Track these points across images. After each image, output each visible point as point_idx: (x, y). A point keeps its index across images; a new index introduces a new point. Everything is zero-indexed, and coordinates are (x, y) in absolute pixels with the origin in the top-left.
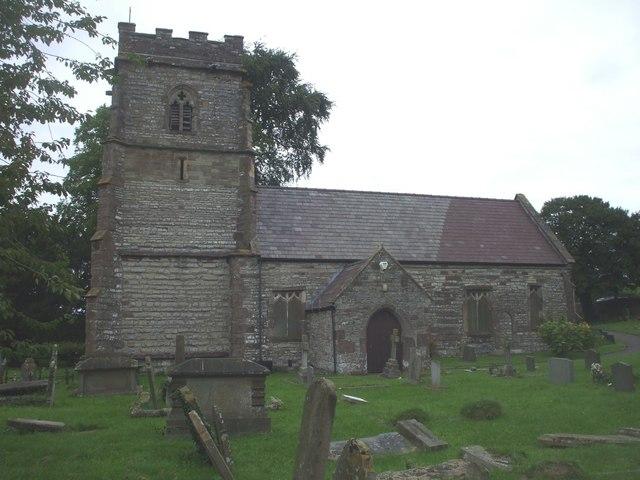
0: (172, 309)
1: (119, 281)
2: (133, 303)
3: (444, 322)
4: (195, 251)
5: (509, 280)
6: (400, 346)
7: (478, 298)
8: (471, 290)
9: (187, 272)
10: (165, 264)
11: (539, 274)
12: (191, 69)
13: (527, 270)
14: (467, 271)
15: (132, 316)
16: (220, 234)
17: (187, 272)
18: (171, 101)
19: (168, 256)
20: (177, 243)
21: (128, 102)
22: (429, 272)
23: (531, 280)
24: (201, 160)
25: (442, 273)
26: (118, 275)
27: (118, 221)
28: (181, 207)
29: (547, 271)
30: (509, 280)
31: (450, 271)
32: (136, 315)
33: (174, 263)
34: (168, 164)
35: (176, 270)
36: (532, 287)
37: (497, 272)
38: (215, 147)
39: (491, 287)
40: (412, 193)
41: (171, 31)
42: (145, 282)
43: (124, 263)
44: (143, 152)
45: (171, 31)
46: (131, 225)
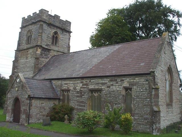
7: (96, 95)
11: (132, 81)
12: (31, 24)
13: (123, 79)
14: (92, 81)
22: (76, 82)
23: (126, 84)
25: (81, 82)
27: (16, 72)
28: (26, 66)
29: (136, 79)
30: (112, 85)
31: (84, 81)
36: (126, 89)
37: (106, 81)
44: (22, 52)
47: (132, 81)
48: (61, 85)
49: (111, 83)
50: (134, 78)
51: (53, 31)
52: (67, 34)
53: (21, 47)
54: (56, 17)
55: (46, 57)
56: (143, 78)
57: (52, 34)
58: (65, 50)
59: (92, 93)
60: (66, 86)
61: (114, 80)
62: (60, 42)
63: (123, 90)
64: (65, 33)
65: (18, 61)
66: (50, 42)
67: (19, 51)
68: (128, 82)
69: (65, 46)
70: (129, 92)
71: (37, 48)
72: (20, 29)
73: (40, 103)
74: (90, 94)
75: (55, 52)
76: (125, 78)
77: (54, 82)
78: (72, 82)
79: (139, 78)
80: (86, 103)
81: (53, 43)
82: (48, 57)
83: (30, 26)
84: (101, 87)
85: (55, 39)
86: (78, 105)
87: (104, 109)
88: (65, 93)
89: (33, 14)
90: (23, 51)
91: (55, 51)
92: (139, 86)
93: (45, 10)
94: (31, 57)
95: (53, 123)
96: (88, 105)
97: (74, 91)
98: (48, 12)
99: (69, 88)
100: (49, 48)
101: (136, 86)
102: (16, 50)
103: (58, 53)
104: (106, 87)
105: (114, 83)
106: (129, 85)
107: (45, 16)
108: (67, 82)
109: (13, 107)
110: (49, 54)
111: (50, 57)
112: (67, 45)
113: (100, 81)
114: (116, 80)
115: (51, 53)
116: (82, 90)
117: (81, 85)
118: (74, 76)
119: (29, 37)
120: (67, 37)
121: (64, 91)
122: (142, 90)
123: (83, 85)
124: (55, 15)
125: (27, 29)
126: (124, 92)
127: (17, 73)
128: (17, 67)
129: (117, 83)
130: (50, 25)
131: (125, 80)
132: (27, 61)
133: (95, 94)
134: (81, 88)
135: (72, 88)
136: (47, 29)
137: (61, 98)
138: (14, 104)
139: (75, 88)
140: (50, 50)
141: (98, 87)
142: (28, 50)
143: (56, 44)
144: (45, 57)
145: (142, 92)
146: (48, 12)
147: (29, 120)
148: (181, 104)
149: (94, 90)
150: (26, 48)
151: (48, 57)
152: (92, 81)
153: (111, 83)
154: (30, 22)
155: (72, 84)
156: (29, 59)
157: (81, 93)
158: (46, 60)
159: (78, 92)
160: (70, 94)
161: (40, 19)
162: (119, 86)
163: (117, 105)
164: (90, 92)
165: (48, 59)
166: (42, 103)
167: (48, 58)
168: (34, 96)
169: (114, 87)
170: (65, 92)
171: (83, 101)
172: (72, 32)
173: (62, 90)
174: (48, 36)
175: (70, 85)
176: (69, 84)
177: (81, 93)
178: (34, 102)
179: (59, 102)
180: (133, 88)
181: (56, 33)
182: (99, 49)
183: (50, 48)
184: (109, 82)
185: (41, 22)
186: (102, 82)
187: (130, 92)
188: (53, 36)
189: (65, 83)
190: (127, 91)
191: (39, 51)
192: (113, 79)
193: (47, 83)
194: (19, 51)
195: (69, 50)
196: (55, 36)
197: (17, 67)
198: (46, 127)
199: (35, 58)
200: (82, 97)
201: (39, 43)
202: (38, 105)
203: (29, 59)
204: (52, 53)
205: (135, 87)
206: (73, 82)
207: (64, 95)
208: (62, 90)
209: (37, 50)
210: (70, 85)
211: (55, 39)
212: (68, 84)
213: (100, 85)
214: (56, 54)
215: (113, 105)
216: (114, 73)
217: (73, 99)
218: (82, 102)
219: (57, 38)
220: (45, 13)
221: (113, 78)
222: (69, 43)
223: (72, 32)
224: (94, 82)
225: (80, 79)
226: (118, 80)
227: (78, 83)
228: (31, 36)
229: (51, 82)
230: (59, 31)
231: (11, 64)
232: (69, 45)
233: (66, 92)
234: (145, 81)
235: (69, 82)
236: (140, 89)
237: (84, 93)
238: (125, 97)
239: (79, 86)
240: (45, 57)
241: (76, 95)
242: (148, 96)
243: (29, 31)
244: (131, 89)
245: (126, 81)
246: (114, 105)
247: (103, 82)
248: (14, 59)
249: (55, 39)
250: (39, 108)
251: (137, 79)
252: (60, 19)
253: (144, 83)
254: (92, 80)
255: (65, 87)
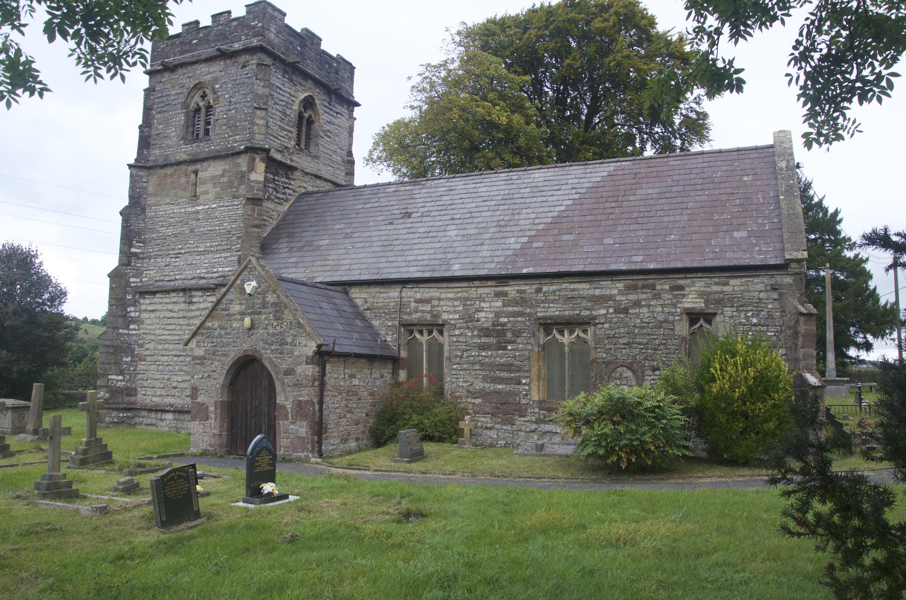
0: (178, 353)
1: (134, 321)
2: (147, 346)
3: (495, 380)
4: (203, 281)
5: (637, 304)
6: (179, 541)
7: (566, 339)
8: (547, 325)
9: (193, 308)
10: (175, 300)
11: (715, 288)
12: (209, 60)
13: (681, 282)
14: (545, 289)
15: (145, 361)
16: (225, 258)
17: (193, 308)
18: (193, 106)
19: (174, 290)
20: (189, 273)
21: (154, 118)
22: (473, 293)
23: (692, 301)
24: (214, 169)
25: (497, 295)
26: (132, 314)
27: (135, 254)
28: (192, 231)
29: (733, 282)
30: (637, 304)
31: (512, 290)
32: (148, 359)
33: (180, 297)
34: (183, 180)
35: (183, 306)
36: (693, 317)
37: (613, 288)
38: (229, 149)
39: (594, 318)
40: (363, 184)
41: (229, 12)
42: (157, 321)
43: (142, 301)
44: (163, 172)
45: (229, 12)
46: (149, 258)
47: (715, 288)
48: (402, 305)
49: (633, 297)
50: (723, 280)
51: (302, 97)
52: (344, 110)
53: (156, 154)
54: (309, 39)
55: (279, 198)
56: (756, 280)
57: (296, 107)
58: (338, 172)
59: (548, 332)
60: (428, 308)
61: (644, 287)
62: (324, 145)
63: (681, 320)
64: (339, 108)
65: (143, 210)
66: (290, 138)
67: (141, 167)
68: (701, 294)
69: (339, 158)
70: (701, 326)
71: (254, 159)
72: (148, 77)
73: (347, 376)
74: (542, 339)
75: (307, 179)
76: (689, 281)
77: (355, 293)
78: (451, 295)
79: (743, 280)
80: (527, 368)
81: (298, 143)
82: (284, 197)
83: (203, 69)
84: (588, 313)
85: (304, 129)
86: (485, 379)
87: (488, 409)
88: (418, 336)
89: (215, 17)
90: (169, 171)
91: (307, 174)
92: (741, 306)
93: (274, 8)
94: (218, 197)
95: (429, 447)
96: (534, 377)
97: (468, 328)
98: (285, 15)
99: (438, 316)
100: (289, 162)
101: (732, 306)
102: (132, 162)
103: (318, 182)
104: (611, 310)
105: (644, 296)
106: (706, 303)
107: (272, 29)
108: (426, 296)
109: (226, 394)
110: (290, 184)
111: (292, 199)
112: (344, 153)
113: (583, 288)
114: (653, 287)
115: (294, 180)
116: (504, 324)
117: (500, 304)
118: (457, 270)
119: (198, 110)
120: (342, 121)
121: (415, 328)
122: (755, 320)
123: (504, 306)
124: (307, 30)
125: (186, 79)
126: (682, 328)
127: (143, 259)
128: (139, 234)
129: (657, 296)
130: (294, 71)
131: (690, 286)
132: (198, 212)
133: (563, 336)
134: (498, 315)
135: (457, 316)
136: (280, 86)
137: (404, 354)
138: (230, 384)
139: (469, 319)
140: (293, 169)
141: (578, 312)
142: (198, 166)
143: (307, 146)
144: (277, 198)
145: (755, 325)
146: (285, 15)
147: (320, 442)
148: (149, 503)
149: (556, 324)
150: (184, 157)
151: (284, 197)
152: (545, 289)
153: (633, 297)
154: (210, 51)
155: (456, 299)
156: (209, 202)
157: (501, 333)
158: (280, 208)
159: (487, 329)
160: (445, 340)
161: (255, 42)
162: (663, 306)
163: (657, 373)
164: (542, 330)
165: (286, 206)
166: (352, 376)
167: (287, 200)
168: (337, 349)
169: (645, 310)
170: (421, 333)
171: (512, 365)
172: (358, 105)
173: (404, 326)
174: (285, 114)
175: (447, 304)
176: (439, 299)
177: (498, 335)
178: (335, 373)
179: (395, 373)
180: (722, 313)
181: (308, 103)
182: (520, 173)
183: (291, 160)
184: (621, 293)
185: (259, 55)
186: (591, 292)
187: (705, 325)
188: (300, 117)
189: (418, 296)
190: (696, 324)
191: (259, 175)
192: (640, 284)
193: (339, 299)
194: (150, 168)
195: (351, 173)
196: (306, 115)
197: (139, 234)
198: (418, 463)
199: (248, 199)
200: (505, 348)
201: (259, 140)
202: (342, 384)
203: (209, 202)
204: (301, 185)
205: (728, 311)
206: (456, 293)
207: (412, 345)
208: (404, 326)
209: (252, 168)
210: (447, 304)
211: (305, 127)
212: (435, 303)
213: (585, 303)
214: (310, 189)
215: (643, 373)
216: (638, 261)
217: (461, 357)
218: (507, 367)
219: (310, 122)
220: (273, 17)
221: (640, 280)
222: (350, 145)
223: (358, 105)
224: (554, 291)
225: (490, 283)
226: (658, 287)
227: (481, 299)
228: (209, 107)
229: (346, 293)
230: (320, 100)
231: (117, 222)
232: (350, 154)
233: (425, 333)
234: (767, 291)
235: (558, 287)
236: (747, 317)
237: (517, 334)
238: (690, 345)
239: (489, 307)
240: (277, 198)
241: (476, 340)
242: (780, 340)
243: (198, 86)
244: (709, 317)
245: (692, 289)
246: (649, 372)
247: (597, 292)
248: (126, 202)
249: (304, 129)
250: (345, 395)
251: (735, 284)
252: (322, 48)
253: (762, 295)
254: (546, 284)
255: (422, 313)
